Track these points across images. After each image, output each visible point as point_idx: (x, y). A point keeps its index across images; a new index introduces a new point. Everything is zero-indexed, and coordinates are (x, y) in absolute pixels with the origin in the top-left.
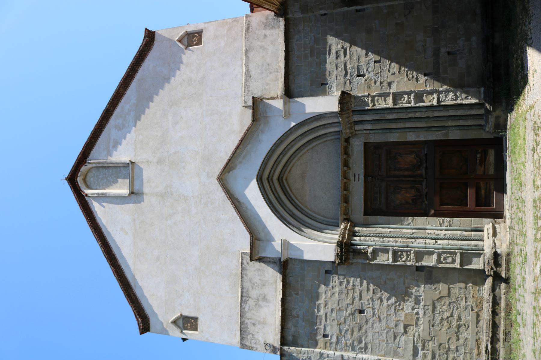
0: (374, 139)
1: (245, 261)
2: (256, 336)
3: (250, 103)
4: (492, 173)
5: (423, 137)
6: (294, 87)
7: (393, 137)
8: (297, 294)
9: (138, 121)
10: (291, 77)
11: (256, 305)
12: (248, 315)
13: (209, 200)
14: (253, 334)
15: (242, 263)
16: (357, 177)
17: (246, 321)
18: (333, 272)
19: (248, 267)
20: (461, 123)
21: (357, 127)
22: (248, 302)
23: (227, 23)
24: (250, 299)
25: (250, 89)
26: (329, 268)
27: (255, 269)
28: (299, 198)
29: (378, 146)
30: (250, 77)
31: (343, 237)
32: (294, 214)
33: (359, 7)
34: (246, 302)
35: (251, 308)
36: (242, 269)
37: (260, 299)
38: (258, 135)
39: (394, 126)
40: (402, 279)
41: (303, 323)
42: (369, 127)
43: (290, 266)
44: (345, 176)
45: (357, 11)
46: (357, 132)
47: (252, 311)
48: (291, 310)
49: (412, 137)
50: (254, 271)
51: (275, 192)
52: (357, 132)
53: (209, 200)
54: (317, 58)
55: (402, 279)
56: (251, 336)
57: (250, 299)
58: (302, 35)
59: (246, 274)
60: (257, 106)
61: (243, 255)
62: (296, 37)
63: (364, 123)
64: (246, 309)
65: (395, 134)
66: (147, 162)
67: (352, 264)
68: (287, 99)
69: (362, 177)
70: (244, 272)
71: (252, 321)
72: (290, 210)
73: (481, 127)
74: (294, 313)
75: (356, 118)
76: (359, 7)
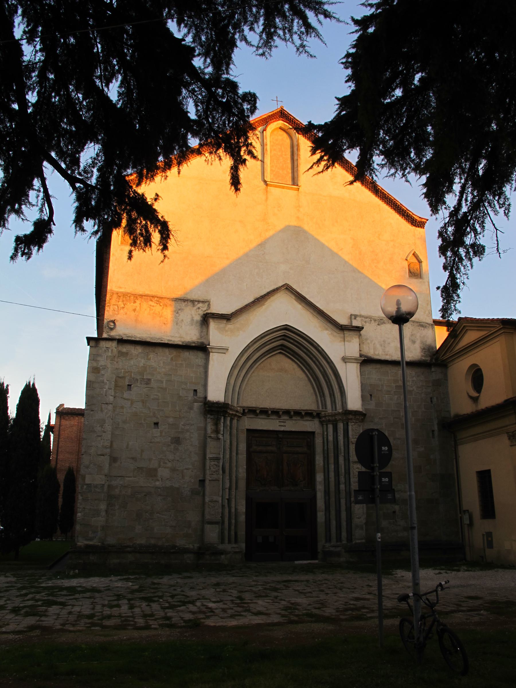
0: (318, 441)
1: (200, 305)
2: (122, 311)
3: (355, 323)
4: (54, 423)
5: (320, 488)
6: (370, 368)
7: (319, 460)
8: (172, 359)
9: (240, 167)
10: (378, 366)
11: (156, 314)
12: (145, 305)
13: (261, 271)
14: (123, 308)
15: (199, 302)
16: (282, 424)
17: (138, 302)
18: (195, 397)
19: (195, 308)
20: (334, 523)
21: (330, 427)
22: (158, 305)
23: (428, 304)
24: (161, 308)
25: (367, 324)
26: (200, 394)
27: (194, 316)
28: (262, 365)
29: (311, 446)
30: (379, 325)
31: (231, 409)
32: (250, 359)
33: (436, 433)
34: (158, 302)
35: (152, 307)
36: (193, 302)
37: (162, 318)
38: (327, 329)
39: (332, 460)
40: (190, 467)
41: (141, 365)
42: (331, 438)
43: (201, 354)
44: (287, 412)
45: (433, 431)
46: (325, 426)
47: (148, 309)
48: (154, 352)
49: (319, 477)
50: (191, 315)
51: (270, 342)
52: (325, 426)
53: (261, 271)
54: (394, 392)
55: (190, 467)
56: (123, 306)
57: (161, 308)
58: (414, 379)
59: (186, 306)
60: (348, 330)
61: (207, 304)
62: (413, 373)
63: (335, 433)
64: (151, 303)
65: (322, 462)
66: (299, 206)
67: (206, 419)
68: (360, 362)
69: (282, 429)
70: (189, 303)
71: (138, 309)
72: (253, 356)
73: (328, 539)
74: (151, 356)
75: (341, 426)
76: (436, 433)
